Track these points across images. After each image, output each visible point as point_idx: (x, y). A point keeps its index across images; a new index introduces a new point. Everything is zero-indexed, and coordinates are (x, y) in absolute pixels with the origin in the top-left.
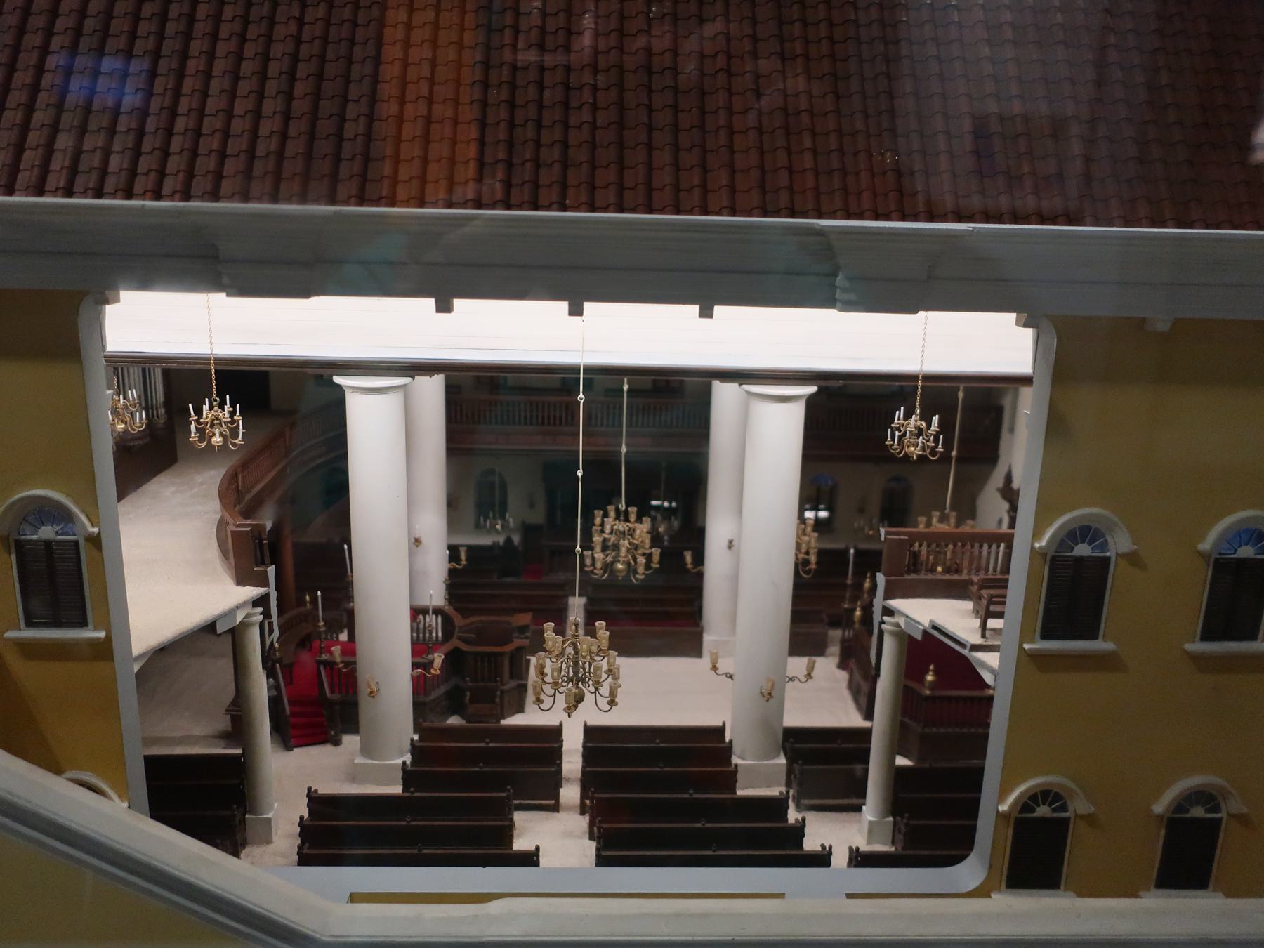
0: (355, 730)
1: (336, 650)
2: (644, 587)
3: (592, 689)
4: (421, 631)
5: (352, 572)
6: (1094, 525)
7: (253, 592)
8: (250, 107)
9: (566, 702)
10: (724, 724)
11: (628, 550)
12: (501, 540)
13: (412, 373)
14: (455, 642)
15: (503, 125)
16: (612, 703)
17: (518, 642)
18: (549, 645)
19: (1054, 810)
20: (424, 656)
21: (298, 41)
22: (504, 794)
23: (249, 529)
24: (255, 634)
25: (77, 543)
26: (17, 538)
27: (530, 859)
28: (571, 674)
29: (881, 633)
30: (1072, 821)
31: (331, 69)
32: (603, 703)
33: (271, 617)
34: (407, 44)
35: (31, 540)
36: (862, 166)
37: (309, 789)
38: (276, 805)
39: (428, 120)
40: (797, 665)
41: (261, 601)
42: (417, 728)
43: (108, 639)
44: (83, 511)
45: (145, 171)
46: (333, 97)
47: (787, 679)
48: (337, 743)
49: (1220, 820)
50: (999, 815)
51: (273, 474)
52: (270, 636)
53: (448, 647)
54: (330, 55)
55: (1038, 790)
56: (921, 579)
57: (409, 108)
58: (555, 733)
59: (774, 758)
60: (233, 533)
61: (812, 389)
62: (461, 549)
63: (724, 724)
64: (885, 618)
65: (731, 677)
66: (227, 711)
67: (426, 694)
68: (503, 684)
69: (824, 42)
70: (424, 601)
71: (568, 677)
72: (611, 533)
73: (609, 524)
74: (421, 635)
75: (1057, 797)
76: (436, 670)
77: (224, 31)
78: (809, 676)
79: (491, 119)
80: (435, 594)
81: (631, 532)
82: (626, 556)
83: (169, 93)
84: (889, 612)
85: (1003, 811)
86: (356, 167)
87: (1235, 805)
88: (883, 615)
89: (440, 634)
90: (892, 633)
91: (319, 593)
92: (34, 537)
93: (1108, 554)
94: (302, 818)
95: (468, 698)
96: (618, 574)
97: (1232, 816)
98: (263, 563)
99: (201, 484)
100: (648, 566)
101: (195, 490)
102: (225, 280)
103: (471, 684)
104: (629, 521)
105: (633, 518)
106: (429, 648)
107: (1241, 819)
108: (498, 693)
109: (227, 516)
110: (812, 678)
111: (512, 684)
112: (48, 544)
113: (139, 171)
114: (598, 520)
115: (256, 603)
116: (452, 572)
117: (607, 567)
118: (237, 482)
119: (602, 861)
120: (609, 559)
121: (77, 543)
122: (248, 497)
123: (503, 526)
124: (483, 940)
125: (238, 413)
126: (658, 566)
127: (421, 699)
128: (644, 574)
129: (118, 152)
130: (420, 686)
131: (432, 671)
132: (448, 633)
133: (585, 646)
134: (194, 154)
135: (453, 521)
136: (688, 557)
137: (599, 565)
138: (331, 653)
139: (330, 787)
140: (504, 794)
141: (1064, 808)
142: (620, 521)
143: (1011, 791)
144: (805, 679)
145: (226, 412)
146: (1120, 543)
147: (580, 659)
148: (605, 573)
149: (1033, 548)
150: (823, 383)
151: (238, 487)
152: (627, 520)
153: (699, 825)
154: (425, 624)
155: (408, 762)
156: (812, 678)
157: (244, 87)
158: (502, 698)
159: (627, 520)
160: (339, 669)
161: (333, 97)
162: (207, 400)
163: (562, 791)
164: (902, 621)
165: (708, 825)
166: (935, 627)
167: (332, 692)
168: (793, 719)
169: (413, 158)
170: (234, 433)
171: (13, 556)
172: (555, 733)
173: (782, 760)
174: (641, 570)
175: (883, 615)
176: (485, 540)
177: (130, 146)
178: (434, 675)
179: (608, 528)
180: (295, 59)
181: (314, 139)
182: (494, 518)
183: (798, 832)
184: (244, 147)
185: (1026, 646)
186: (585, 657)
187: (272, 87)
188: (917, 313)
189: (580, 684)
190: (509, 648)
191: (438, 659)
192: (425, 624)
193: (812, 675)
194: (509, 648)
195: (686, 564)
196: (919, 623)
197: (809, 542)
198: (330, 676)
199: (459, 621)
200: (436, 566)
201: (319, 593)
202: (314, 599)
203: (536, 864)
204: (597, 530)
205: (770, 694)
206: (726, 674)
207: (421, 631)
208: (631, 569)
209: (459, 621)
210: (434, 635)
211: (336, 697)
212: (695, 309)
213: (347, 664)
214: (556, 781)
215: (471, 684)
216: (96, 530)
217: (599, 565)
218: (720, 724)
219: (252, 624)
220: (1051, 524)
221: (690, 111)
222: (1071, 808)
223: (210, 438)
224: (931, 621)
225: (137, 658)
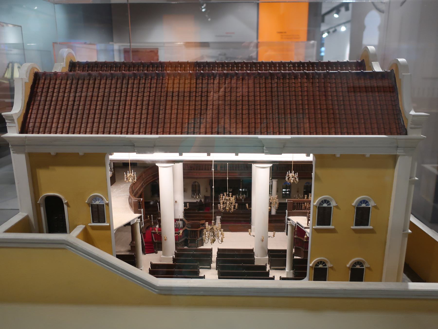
0: (161, 250)
1: (157, 229)
2: (233, 213)
3: (217, 238)
4: (177, 225)
5: (160, 211)
6: (327, 200)
7: (138, 215)
8: (140, 112)
9: (211, 241)
10: (253, 248)
11: (229, 204)
12: (199, 200)
13: (174, 163)
14: (186, 228)
15: (193, 114)
16: (222, 241)
17: (201, 228)
18: (207, 227)
19: (323, 266)
20: (178, 231)
21: (149, 96)
22: (197, 264)
23: (137, 200)
24: (138, 225)
25: (104, 205)
26: (91, 204)
27: (203, 277)
28: (212, 234)
29: (287, 225)
30: (328, 268)
31: (157, 103)
32: (220, 242)
33: (142, 221)
34: (173, 96)
35: (94, 204)
36: (271, 122)
37: (151, 262)
38: (143, 266)
39: (177, 114)
40: (271, 234)
41: (140, 217)
42: (176, 249)
43: (110, 225)
44: (105, 198)
45: (124, 132)
46: (157, 109)
47: (268, 237)
48: (156, 253)
49: (364, 268)
50: (310, 267)
51: (140, 185)
52: (142, 225)
53: (184, 229)
54: (156, 99)
55: (319, 261)
56: (297, 212)
57: (173, 111)
58: (211, 250)
59: (265, 257)
60: (134, 201)
61: (271, 165)
62: (187, 203)
63: (253, 248)
64: (288, 221)
65: (254, 236)
66: (130, 244)
67: (178, 241)
68: (198, 239)
69: (264, 92)
70: (178, 217)
71: (211, 235)
72: (225, 200)
73: (223, 198)
74: (177, 226)
75: (324, 263)
76: (181, 234)
77: (134, 95)
78: (274, 236)
79: (190, 113)
80: (181, 215)
81: (230, 199)
82: (229, 206)
83: (123, 110)
84: (289, 220)
85: (311, 266)
86: (162, 125)
87: (366, 265)
88: (287, 220)
89: (182, 226)
90: (290, 225)
91: (152, 215)
92: (95, 203)
93: (331, 206)
94: (149, 268)
95: (189, 242)
96: (227, 210)
97: (366, 268)
98: (140, 208)
99: (122, 188)
100: (234, 208)
101: (121, 189)
102: (136, 151)
103: (190, 238)
104: (230, 197)
105: (231, 196)
106: (179, 229)
107: (369, 268)
108: (197, 241)
109: (131, 196)
110: (274, 236)
111: (200, 238)
112: (98, 205)
113: (123, 132)
114: (221, 197)
115: (139, 218)
116: (185, 210)
117: (224, 208)
118: (132, 188)
119: (219, 278)
120: (224, 206)
121: (104, 205)
122: (135, 192)
123: (198, 197)
124: (190, 286)
125: (135, 174)
126: (237, 208)
127: (177, 242)
128: (233, 210)
129: (113, 123)
130: (177, 238)
131: (180, 234)
132: (184, 226)
133: (215, 228)
134: (129, 123)
135: (185, 196)
136: (247, 205)
137: (222, 208)
138: (155, 230)
139: (155, 262)
140: (197, 264)
141: (325, 265)
142: (227, 196)
143: (312, 261)
144: (273, 237)
145: (133, 174)
146: (333, 204)
147: (214, 231)
148: (223, 210)
149: (313, 204)
150: (274, 163)
151: (133, 189)
152: (229, 196)
153: (244, 271)
154: (178, 223)
155: (174, 257)
156: (274, 236)
157: (138, 107)
158: (197, 242)
159: (229, 196)
160: (157, 234)
161: (157, 109)
162: (128, 171)
163: (212, 265)
164: (291, 221)
165: (246, 271)
166: (298, 223)
167: (155, 240)
168: (270, 248)
169: (174, 123)
170: (134, 178)
171: (90, 208)
172: (211, 250)
173: (267, 257)
174: (232, 209)
175: (287, 220)
176: (195, 201)
177: (116, 122)
178: (180, 236)
179: (224, 199)
180: (149, 100)
181: (153, 119)
182: (196, 195)
183: (268, 273)
184: (139, 121)
185: (313, 227)
186: (215, 230)
187: (144, 107)
188: (282, 154)
189: (215, 237)
190: (199, 229)
191: (181, 232)
192: (178, 223)
193: (275, 236)
194: (199, 229)
195: (247, 207)
196: (295, 222)
197: (276, 201)
198: (155, 236)
199: (187, 222)
200: (181, 208)
201: (152, 215)
202: (150, 217)
203: (205, 278)
204: (221, 199)
205: (263, 240)
206: (253, 235)
207: (177, 225)
208: (230, 209)
209: (187, 222)
210: (180, 226)
211: (156, 241)
212: (234, 154)
213: (159, 233)
214: (210, 262)
215: (190, 238)
216: (108, 202)
217: (222, 208)
218: (252, 248)
219: (138, 223)
220: (317, 199)
221: (234, 110)
222: (327, 265)
223: (129, 180)
224: (297, 222)
225: (115, 230)
